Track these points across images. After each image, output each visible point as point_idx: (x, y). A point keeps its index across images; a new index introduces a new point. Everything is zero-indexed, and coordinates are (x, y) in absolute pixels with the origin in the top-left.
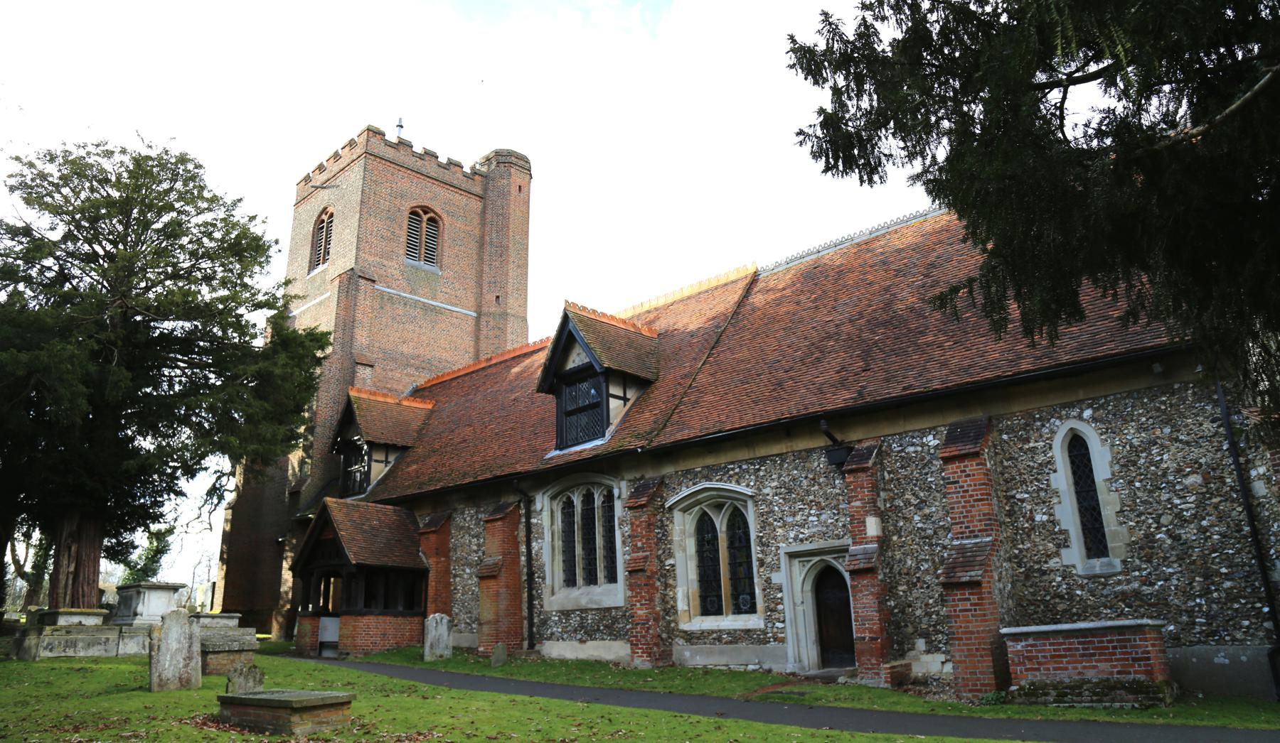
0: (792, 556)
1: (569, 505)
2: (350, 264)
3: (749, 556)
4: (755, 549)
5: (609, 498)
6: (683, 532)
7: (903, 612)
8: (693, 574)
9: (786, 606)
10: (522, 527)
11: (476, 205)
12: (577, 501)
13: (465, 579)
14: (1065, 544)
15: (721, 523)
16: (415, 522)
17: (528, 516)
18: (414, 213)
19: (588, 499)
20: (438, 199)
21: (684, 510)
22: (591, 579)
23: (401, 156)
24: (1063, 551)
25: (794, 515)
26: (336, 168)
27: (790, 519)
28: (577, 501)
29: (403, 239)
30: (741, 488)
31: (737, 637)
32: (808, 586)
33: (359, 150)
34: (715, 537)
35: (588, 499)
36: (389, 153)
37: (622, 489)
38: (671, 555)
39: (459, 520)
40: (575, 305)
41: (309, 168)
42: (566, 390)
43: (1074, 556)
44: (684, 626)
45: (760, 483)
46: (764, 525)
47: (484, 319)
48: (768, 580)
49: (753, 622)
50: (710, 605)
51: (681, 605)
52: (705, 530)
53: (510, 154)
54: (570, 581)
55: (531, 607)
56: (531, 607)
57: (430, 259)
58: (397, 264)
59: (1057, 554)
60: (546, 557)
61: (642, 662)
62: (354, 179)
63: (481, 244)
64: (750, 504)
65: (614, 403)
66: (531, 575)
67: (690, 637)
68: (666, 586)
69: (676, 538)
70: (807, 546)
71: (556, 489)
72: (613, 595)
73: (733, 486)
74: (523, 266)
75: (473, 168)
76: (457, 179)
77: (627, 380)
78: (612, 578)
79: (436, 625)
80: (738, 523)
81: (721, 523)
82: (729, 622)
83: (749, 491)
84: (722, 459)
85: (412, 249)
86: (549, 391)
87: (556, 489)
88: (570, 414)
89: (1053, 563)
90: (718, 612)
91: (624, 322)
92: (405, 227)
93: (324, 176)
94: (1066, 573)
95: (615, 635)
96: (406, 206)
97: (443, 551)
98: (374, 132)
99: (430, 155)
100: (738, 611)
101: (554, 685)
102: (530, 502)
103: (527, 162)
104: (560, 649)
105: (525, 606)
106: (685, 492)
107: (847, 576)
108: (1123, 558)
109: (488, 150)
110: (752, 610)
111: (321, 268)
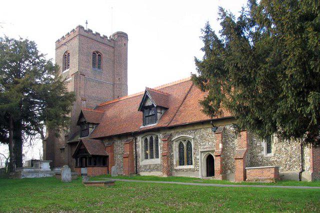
0: (202, 152)
1: (146, 139)
2: (77, 70)
3: (191, 152)
4: (193, 151)
5: (157, 137)
6: (175, 146)
7: (226, 164)
8: (178, 156)
9: (199, 164)
10: (134, 145)
11: (112, 50)
12: (148, 138)
13: (119, 158)
14: (262, 150)
15: (185, 144)
16: (104, 144)
17: (136, 143)
18: (93, 53)
19: (151, 138)
20: (101, 49)
21: (176, 141)
22: (152, 157)
23: (89, 35)
24: (262, 152)
25: (203, 143)
26: (69, 39)
27: (202, 144)
28: (148, 138)
29: (91, 62)
30: (191, 136)
31: (187, 170)
32: (205, 159)
33: (76, 33)
34: (184, 148)
35: (151, 138)
36: (86, 34)
37: (161, 136)
38: (173, 152)
39: (116, 143)
40: (148, 88)
41: (60, 38)
42: (145, 111)
43: (264, 152)
44: (175, 168)
45: (195, 135)
46: (195, 145)
47: (115, 85)
48: (196, 158)
49: (192, 167)
50: (181, 163)
51: (175, 163)
52: (181, 145)
53: (122, 33)
54: (146, 158)
55: (136, 165)
56: (136, 165)
57: (99, 68)
58: (89, 70)
59: (261, 152)
60: (140, 152)
61: (165, 176)
62: (76, 42)
63: (114, 62)
64: (192, 140)
65: (158, 114)
66: (136, 157)
67: (176, 170)
68: (171, 159)
69: (174, 148)
70: (205, 150)
71: (143, 136)
72: (158, 161)
73: (188, 136)
74: (126, 69)
75: (110, 37)
76: (106, 42)
77: (161, 108)
78: (157, 157)
79: (113, 169)
80: (189, 143)
81: (185, 144)
82: (186, 167)
83: (192, 137)
84: (186, 129)
85: (94, 64)
86: (141, 111)
87: (143, 136)
88: (146, 117)
89: (260, 154)
90: (183, 165)
91: (158, 91)
92: (92, 58)
93: (65, 41)
94: (262, 157)
95: (157, 170)
96: (92, 51)
97: (112, 151)
98: (81, 27)
99: (98, 34)
100: (188, 164)
101: (302, 165)
102: (136, 139)
103: (127, 35)
104: (142, 174)
105: (135, 164)
106: (177, 137)
107: (214, 157)
108: (233, 174)
109: (115, 31)
110: (192, 164)
111: (67, 70)
